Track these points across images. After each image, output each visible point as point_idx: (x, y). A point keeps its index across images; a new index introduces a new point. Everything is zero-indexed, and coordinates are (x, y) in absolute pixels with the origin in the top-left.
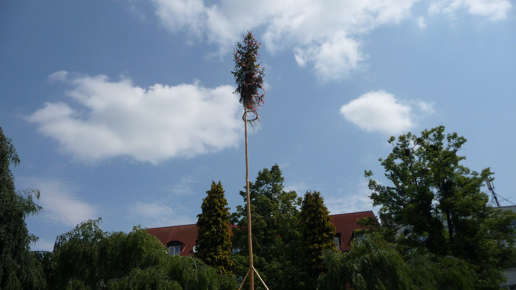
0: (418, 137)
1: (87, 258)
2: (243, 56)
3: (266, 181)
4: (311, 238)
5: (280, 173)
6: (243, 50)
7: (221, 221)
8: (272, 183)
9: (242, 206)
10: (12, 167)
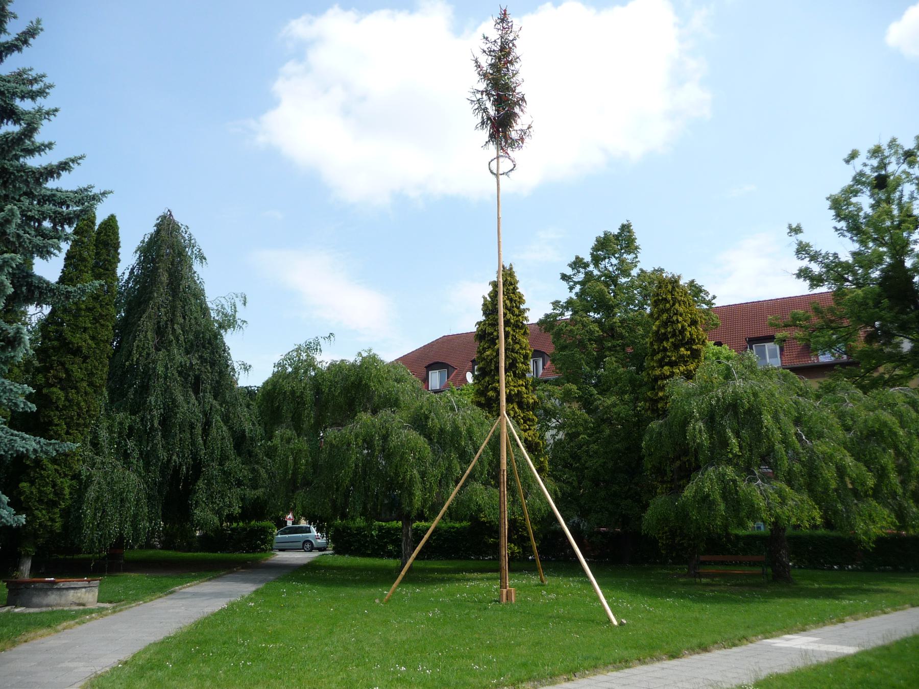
0: (906, 148)
1: (297, 399)
4: (659, 357)
7: (511, 332)
9: (560, 302)
10: (196, 266)
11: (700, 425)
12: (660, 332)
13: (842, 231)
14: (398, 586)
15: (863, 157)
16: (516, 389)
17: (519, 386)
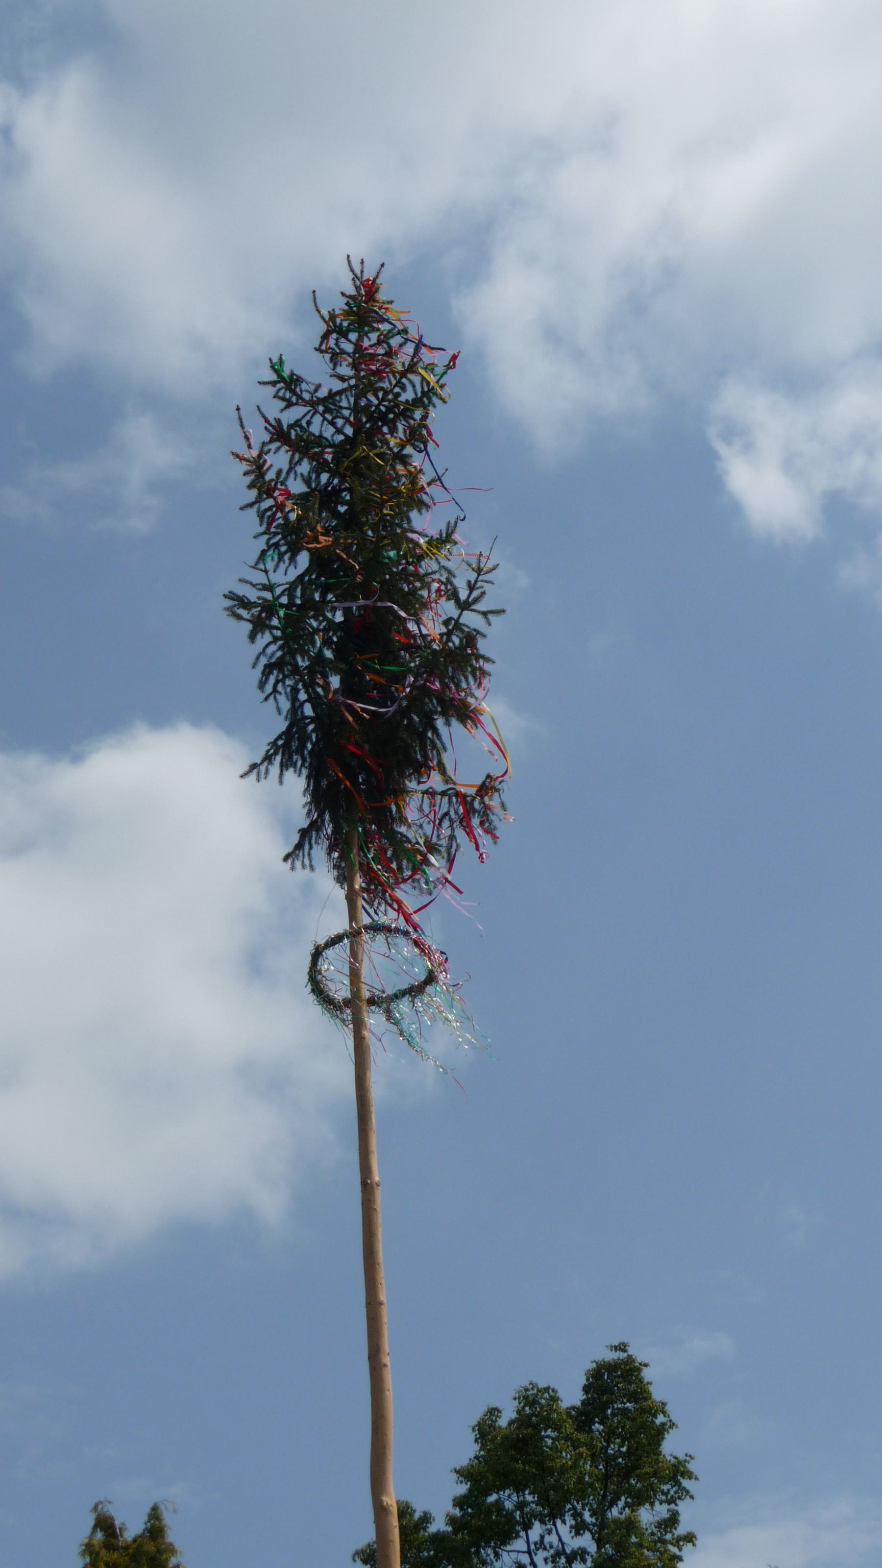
2: (321, 466)
3: (543, 1500)
5: (660, 1419)
6: (318, 419)
8: (593, 1513)
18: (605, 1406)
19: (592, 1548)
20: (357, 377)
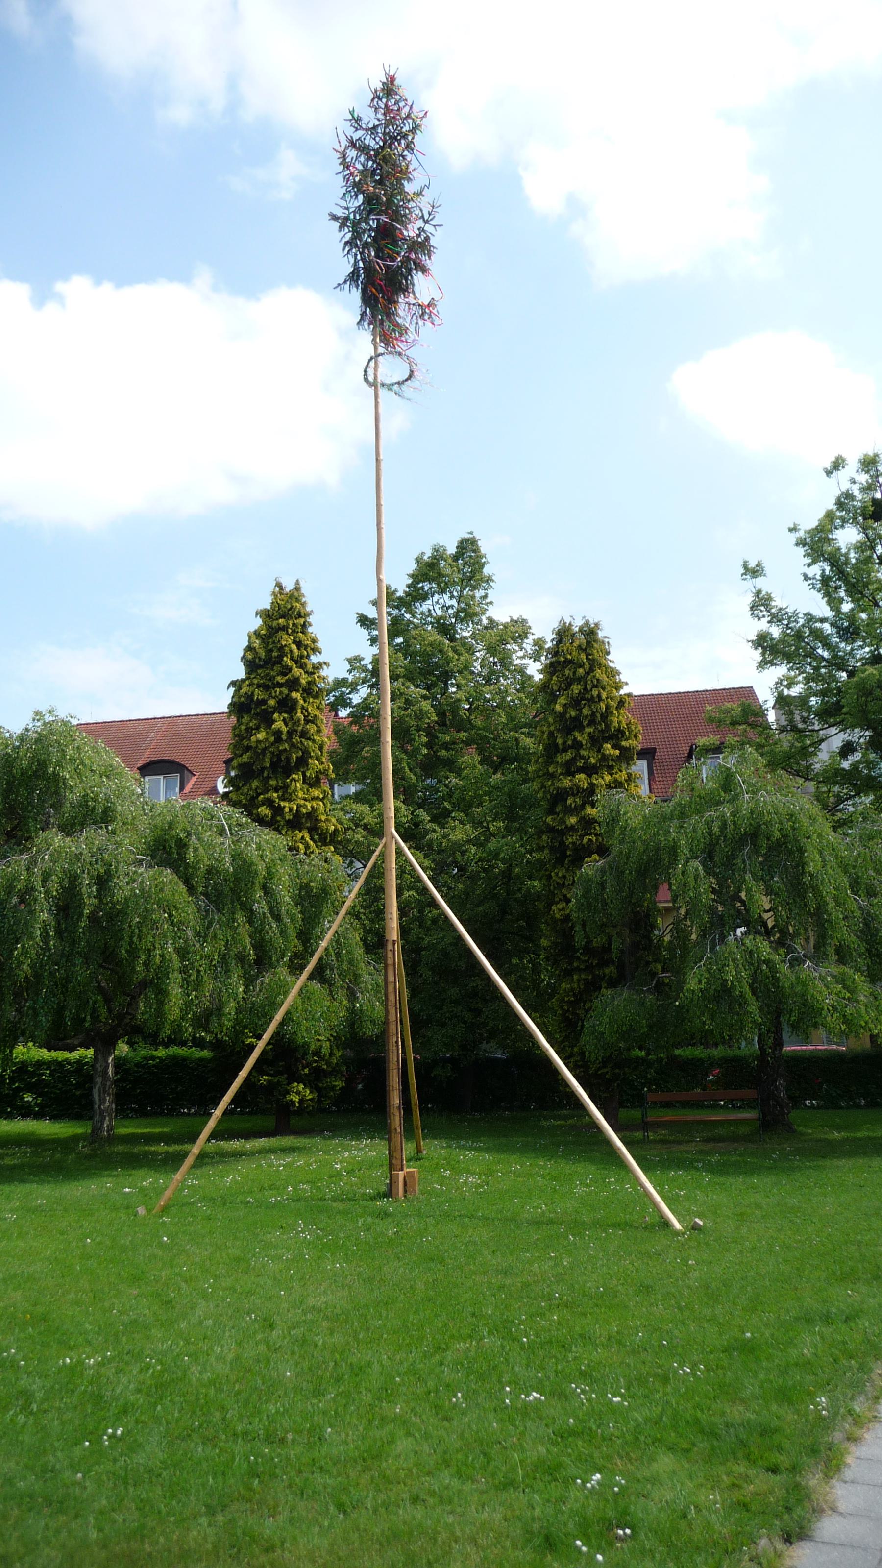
2: (369, 158)
4: (568, 758)
5: (484, 560)
7: (302, 702)
11: (696, 865)
12: (568, 715)
13: (814, 581)
14: (188, 1173)
15: (852, 468)
16: (309, 805)
17: (313, 799)
18: (463, 554)
19: (456, 605)
20: (386, 119)
